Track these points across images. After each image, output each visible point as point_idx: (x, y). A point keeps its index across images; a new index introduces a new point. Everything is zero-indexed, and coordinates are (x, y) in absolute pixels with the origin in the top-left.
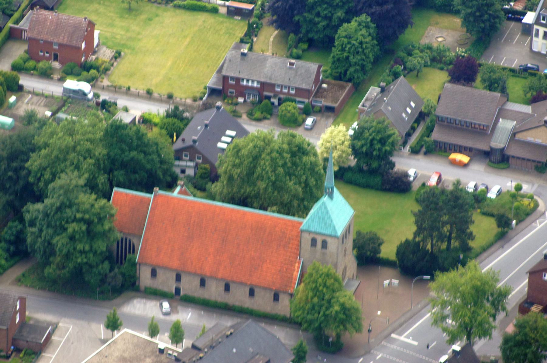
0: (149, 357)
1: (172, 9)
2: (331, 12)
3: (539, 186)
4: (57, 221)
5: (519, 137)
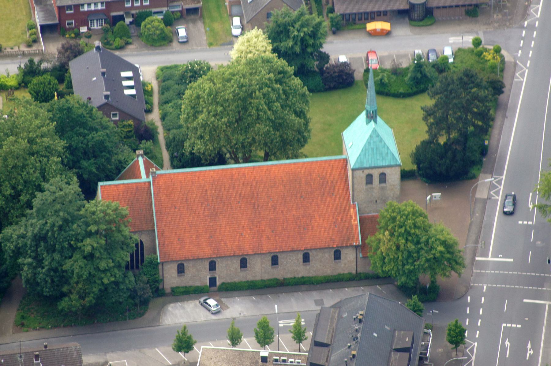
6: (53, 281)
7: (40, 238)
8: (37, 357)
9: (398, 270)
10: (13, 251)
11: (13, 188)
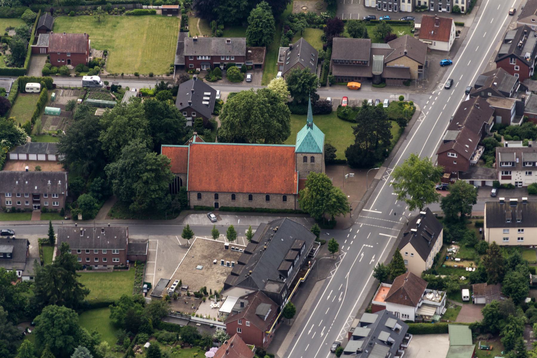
0: (220, 253)
1: (126, 17)
2: (238, 2)
3: (410, 95)
4: (131, 172)
5: (389, 65)
7: (123, 170)
9: (311, 209)
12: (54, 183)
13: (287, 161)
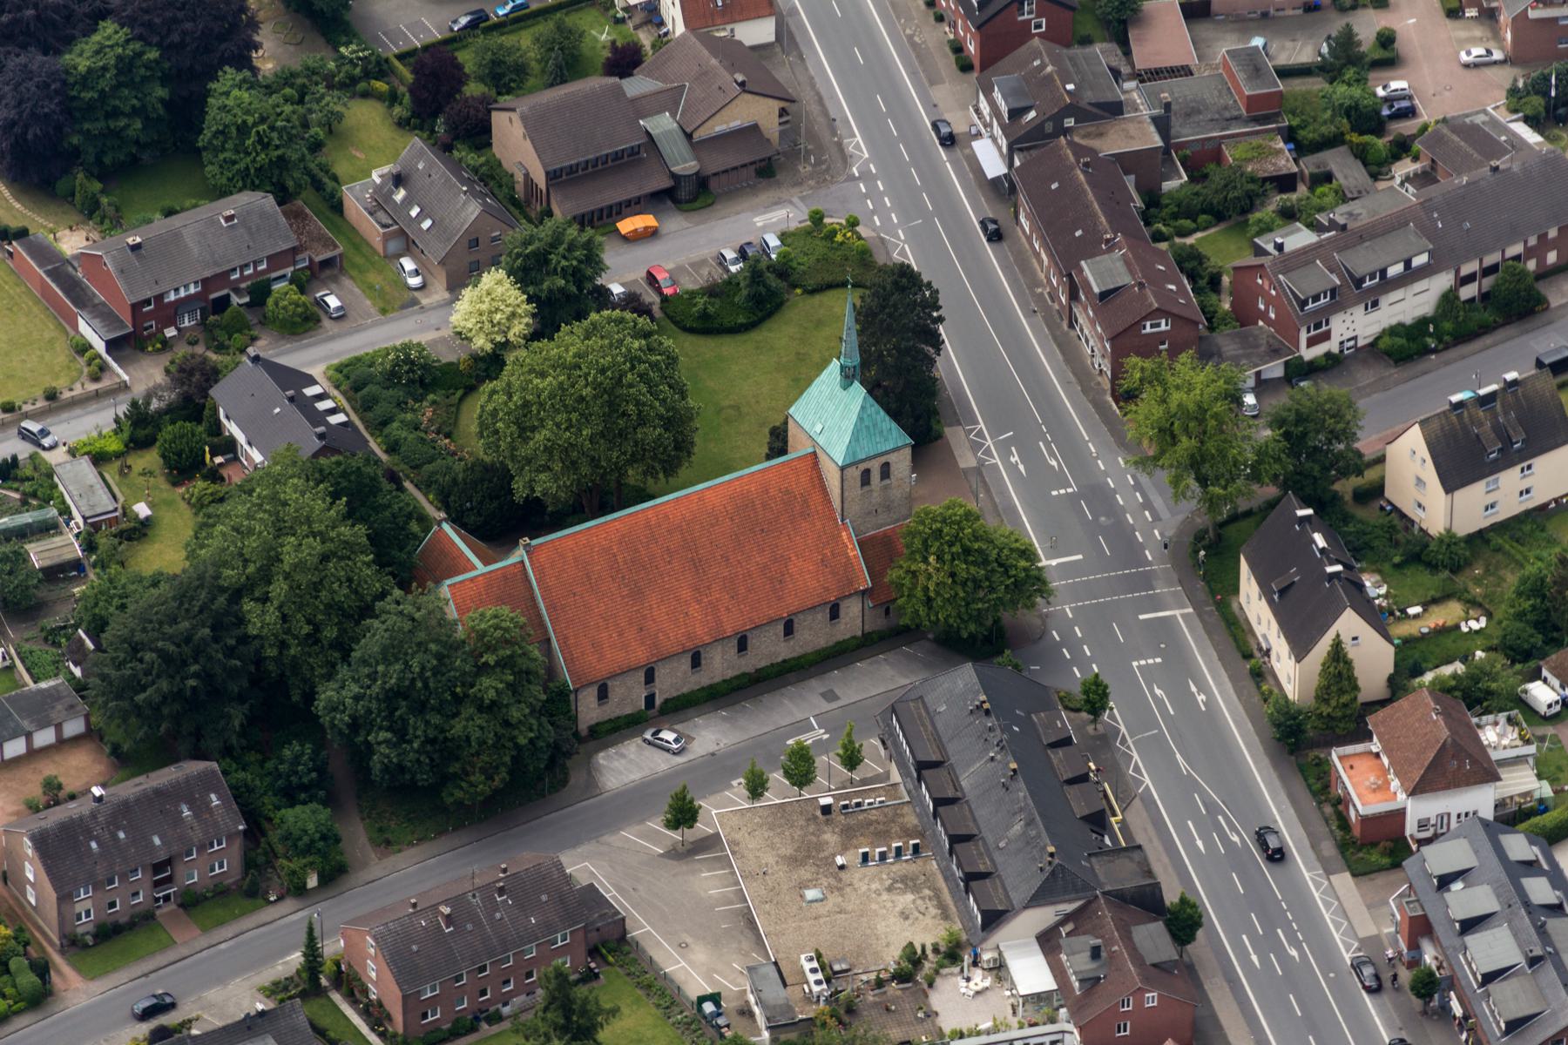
6: (432, 760)
8: (501, 891)
10: (348, 726)
11: (309, 622)
12: (200, 808)
13: (806, 501)
